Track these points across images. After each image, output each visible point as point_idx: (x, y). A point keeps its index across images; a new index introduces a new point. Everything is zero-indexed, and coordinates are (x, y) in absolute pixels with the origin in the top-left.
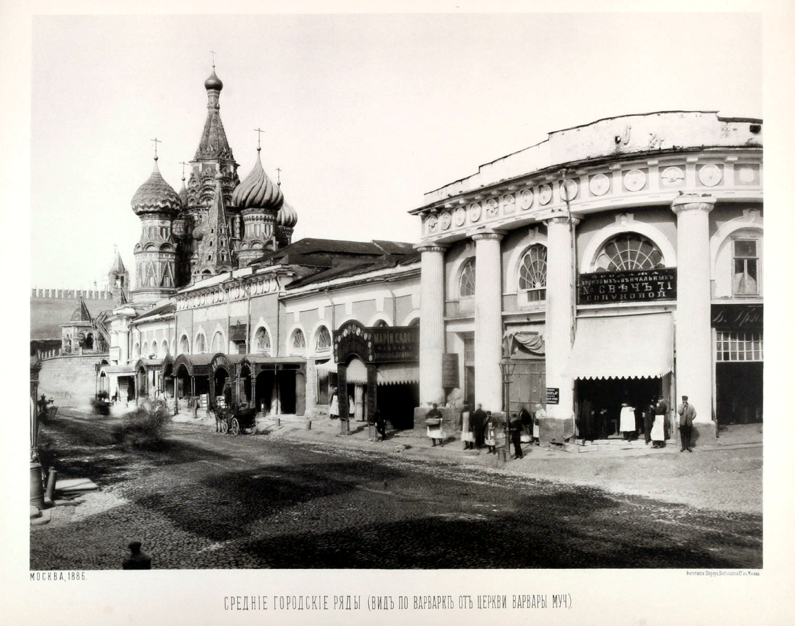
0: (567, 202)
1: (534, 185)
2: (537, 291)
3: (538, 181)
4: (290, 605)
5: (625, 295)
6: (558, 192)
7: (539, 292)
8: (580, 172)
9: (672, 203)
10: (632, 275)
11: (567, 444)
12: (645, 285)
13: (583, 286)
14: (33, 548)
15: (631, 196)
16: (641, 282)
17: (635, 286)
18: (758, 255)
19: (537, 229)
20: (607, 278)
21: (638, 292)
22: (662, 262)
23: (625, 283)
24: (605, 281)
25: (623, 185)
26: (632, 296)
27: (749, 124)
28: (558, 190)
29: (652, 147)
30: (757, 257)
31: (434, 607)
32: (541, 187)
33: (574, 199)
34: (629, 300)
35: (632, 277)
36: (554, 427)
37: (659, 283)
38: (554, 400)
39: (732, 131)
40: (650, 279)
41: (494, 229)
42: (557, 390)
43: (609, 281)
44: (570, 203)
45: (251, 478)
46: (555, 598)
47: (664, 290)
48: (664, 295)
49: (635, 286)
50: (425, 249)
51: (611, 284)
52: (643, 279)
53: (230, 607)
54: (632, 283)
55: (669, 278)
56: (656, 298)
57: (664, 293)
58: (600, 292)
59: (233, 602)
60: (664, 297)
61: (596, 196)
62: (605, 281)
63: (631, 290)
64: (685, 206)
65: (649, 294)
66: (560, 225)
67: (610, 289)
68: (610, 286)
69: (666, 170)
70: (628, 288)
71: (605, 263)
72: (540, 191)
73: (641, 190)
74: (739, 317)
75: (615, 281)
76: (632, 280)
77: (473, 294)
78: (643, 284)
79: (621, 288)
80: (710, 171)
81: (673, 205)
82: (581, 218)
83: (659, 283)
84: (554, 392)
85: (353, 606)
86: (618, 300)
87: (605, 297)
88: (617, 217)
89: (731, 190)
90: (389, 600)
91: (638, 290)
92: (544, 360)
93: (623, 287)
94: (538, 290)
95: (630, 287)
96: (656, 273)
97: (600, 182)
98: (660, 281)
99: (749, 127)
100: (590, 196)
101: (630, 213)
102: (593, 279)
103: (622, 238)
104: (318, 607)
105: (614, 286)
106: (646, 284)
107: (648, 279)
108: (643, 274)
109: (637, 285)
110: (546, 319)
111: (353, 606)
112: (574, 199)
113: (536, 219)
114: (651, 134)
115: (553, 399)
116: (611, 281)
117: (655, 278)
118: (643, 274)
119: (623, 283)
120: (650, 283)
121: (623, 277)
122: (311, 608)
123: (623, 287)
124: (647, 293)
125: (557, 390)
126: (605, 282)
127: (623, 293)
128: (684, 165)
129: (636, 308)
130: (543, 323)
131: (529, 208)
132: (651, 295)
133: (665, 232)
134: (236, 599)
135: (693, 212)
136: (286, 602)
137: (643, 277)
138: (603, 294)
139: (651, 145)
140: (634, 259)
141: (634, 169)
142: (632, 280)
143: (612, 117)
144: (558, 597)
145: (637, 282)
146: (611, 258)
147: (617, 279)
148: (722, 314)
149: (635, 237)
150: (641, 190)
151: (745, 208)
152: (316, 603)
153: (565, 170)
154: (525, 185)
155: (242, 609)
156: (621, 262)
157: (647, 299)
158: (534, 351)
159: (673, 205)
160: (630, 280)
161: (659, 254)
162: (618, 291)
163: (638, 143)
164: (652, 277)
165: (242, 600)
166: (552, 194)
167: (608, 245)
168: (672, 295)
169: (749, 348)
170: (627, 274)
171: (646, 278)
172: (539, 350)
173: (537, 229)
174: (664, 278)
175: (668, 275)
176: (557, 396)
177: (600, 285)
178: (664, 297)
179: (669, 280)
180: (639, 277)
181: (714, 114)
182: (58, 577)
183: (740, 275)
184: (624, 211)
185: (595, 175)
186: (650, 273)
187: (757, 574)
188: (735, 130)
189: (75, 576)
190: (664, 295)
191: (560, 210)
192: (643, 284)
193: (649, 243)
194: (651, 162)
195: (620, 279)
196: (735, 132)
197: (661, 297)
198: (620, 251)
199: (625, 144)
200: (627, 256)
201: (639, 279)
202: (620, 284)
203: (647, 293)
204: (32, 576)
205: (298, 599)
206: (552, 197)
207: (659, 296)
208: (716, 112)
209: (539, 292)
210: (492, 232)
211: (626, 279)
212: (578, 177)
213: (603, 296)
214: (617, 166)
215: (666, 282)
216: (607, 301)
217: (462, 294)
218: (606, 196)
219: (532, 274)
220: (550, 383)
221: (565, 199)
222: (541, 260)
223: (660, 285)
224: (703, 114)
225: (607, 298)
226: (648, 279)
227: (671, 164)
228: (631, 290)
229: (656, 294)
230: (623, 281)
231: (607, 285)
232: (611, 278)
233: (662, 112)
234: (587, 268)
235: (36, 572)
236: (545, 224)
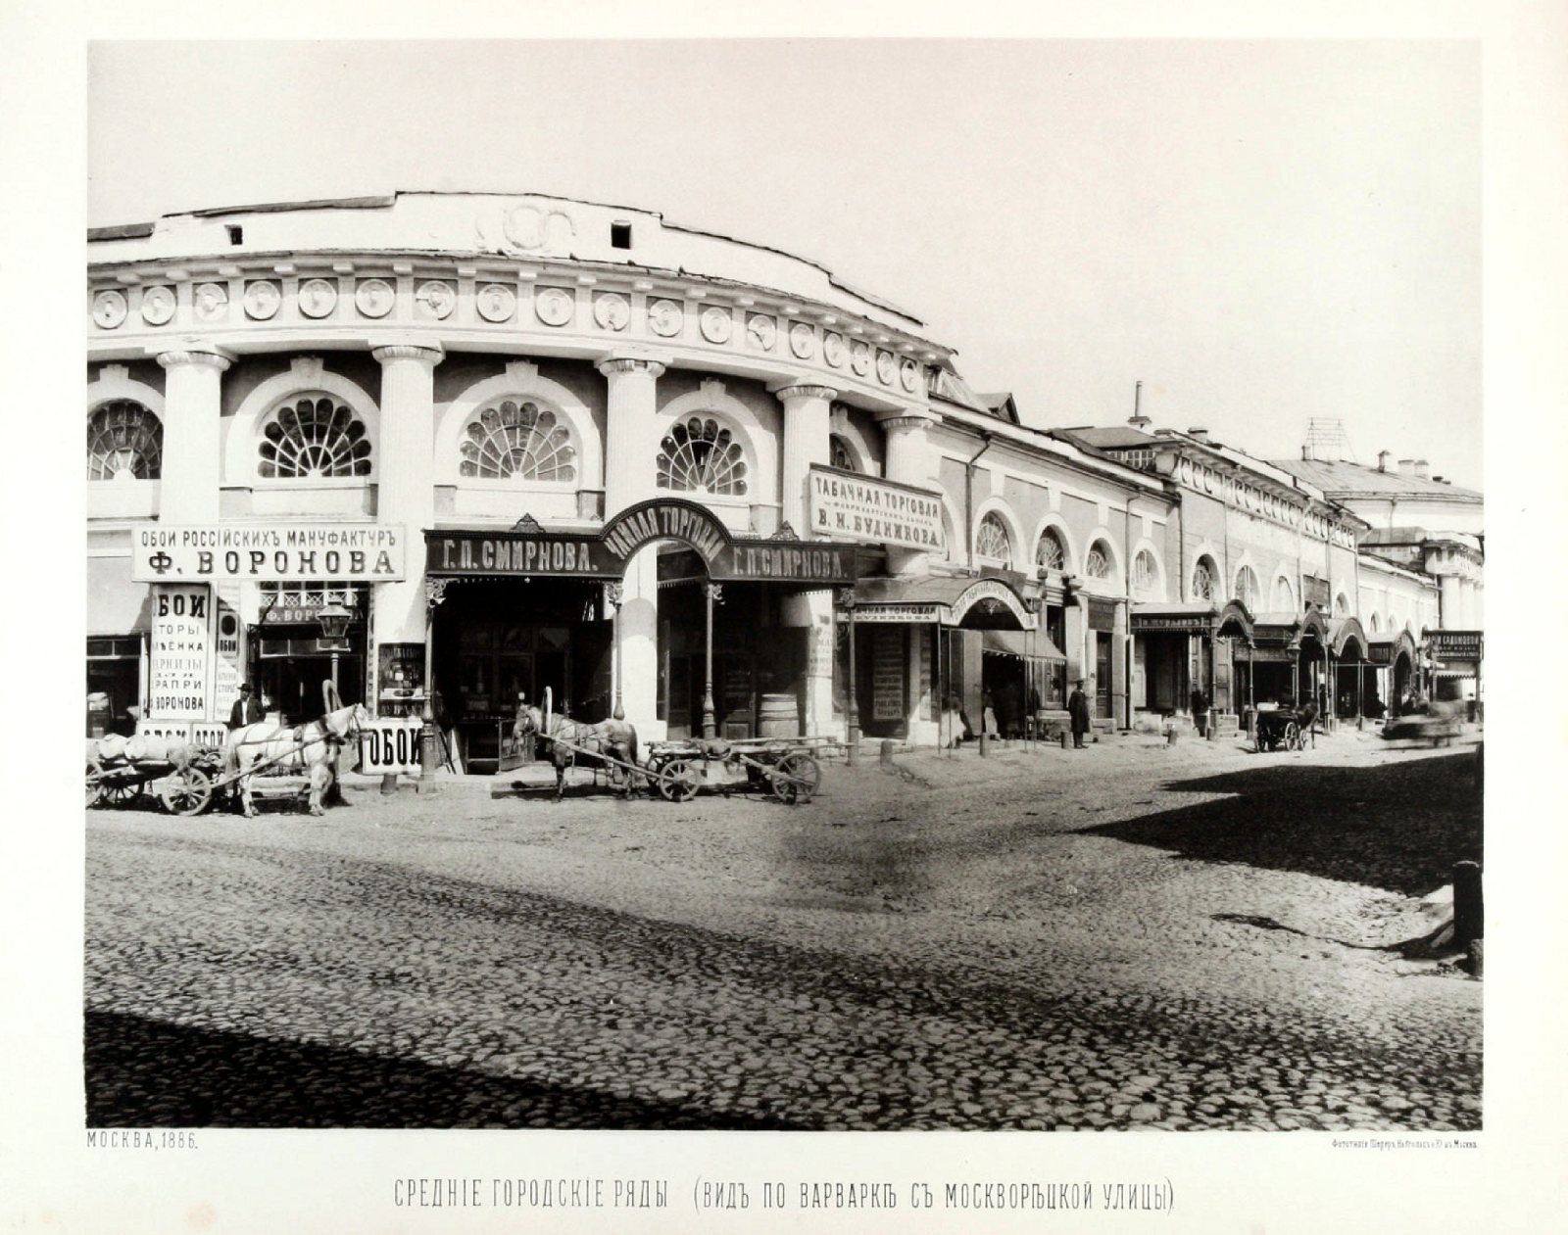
4: (525, 1199)
9: (795, 379)
14: (100, 997)
28: (526, 300)
41: (222, 348)
45: (1181, 850)
46: (951, 1191)
50: (413, 350)
53: (405, 1202)
77: (461, 472)
88: (703, 384)
90: (739, 1189)
104: (583, 1202)
111: (738, 1204)
134: (418, 1184)
136: (511, 1192)
152: (583, 1193)
165: (429, 1187)
166: (338, 300)
169: (880, 688)
182: (143, 1142)
187: (1473, 1145)
189: (177, 1139)
210: (214, 351)
217: (468, 468)
235: (98, 1131)
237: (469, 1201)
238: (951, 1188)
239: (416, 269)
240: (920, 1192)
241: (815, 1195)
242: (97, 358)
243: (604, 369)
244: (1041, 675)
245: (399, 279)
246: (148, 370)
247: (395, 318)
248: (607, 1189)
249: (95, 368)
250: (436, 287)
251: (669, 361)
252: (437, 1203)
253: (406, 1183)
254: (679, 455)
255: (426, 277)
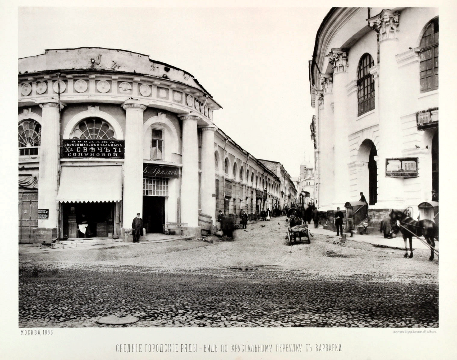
0: (59, 94)
1: (33, 81)
2: (28, 149)
3: (36, 79)
4: (155, 350)
5: (93, 154)
6: (53, 87)
7: (29, 150)
8: (69, 76)
10: (98, 142)
11: (54, 244)
12: (106, 149)
13: (65, 147)
15: (100, 95)
16: (104, 147)
17: (100, 149)
18: (163, 139)
19: (30, 109)
20: (82, 143)
21: (101, 152)
22: (114, 137)
23: (94, 147)
24: (81, 144)
25: (74, 89)
26: (98, 155)
27: (164, 66)
29: (113, 69)
30: (163, 139)
31: (249, 351)
32: (38, 83)
33: (63, 92)
34: (95, 157)
35: (98, 143)
36: (44, 233)
37: (114, 148)
38: (45, 217)
39: (156, 68)
40: (109, 145)
42: (47, 210)
43: (83, 145)
44: (60, 94)
47: (117, 153)
48: (116, 156)
49: (100, 149)
51: (84, 147)
52: (105, 145)
54: (98, 147)
55: (120, 145)
56: (112, 157)
57: (116, 154)
58: (77, 151)
59: (120, 348)
60: (116, 157)
61: (78, 92)
62: (81, 144)
63: (97, 151)
64: (133, 105)
65: (108, 154)
66: (52, 108)
67: (84, 149)
68: (84, 148)
69: (122, 83)
70: (95, 150)
71: (79, 134)
72: (37, 85)
73: (106, 93)
74: (155, 171)
75: (87, 145)
76: (98, 145)
78: (105, 148)
79: (91, 149)
80: (145, 89)
81: (125, 104)
82: (66, 105)
83: (114, 148)
84: (45, 212)
85: (193, 350)
86: (89, 156)
87: (80, 154)
89: (155, 100)
90: (214, 346)
91: (101, 151)
92: (38, 192)
93: (92, 149)
94: (28, 149)
95: (97, 149)
96: (112, 142)
97: (81, 84)
98: (115, 147)
99: (164, 68)
100: (53, 93)
101: (97, 106)
102: (73, 143)
103: (90, 120)
104: (172, 351)
105: (87, 148)
106: (107, 148)
107: (108, 145)
108: (105, 142)
109: (101, 148)
110: (40, 166)
112: (63, 92)
113: (35, 103)
114: (113, 61)
115: (44, 216)
116: (85, 145)
117: (112, 145)
118: (105, 142)
119: (92, 147)
120: (109, 148)
121: (92, 143)
122: (168, 351)
123: (92, 149)
124: (106, 154)
125: (47, 210)
126: (81, 145)
127: (92, 153)
128: (111, 81)
129: (99, 162)
130: (37, 168)
131: (29, 95)
132: (109, 155)
133: (118, 120)
135: (137, 109)
137: (105, 144)
138: (79, 152)
139: (113, 68)
140: (97, 134)
141: (81, 79)
142: (98, 145)
143: (142, 53)
144: (269, 346)
145: (101, 147)
146: (83, 132)
147: (89, 144)
148: (146, 169)
149: (99, 120)
150: (106, 93)
151: (160, 112)
153: (59, 73)
154: (27, 80)
155: (127, 352)
156: (89, 135)
157: (107, 157)
158: (28, 187)
159: (125, 104)
160: (97, 145)
161: (112, 132)
162: (89, 151)
163: (106, 64)
164: (110, 144)
165: (126, 347)
167: (81, 124)
168: (121, 156)
170: (95, 141)
171: (106, 144)
172: (29, 186)
173: (30, 109)
174: (117, 145)
175: (120, 144)
176: (47, 214)
177: (77, 147)
178: (116, 157)
179: (120, 147)
180: (102, 144)
181: (148, 57)
183: (154, 148)
184: (94, 104)
185: (77, 80)
186: (109, 142)
188: (157, 68)
190: (116, 156)
191: (53, 98)
192: (105, 148)
193: (107, 125)
194: (114, 77)
195: (91, 144)
196: (157, 69)
197: (115, 156)
198: (88, 128)
199: (98, 64)
200: (93, 132)
201: (102, 145)
202: (91, 147)
203: (106, 154)
204: (22, 332)
205: (152, 345)
206: (47, 90)
207: (114, 155)
208: (149, 56)
209: (29, 150)
211: (95, 144)
212: (89, 79)
213: (79, 154)
214: (93, 76)
215: (118, 148)
216: (82, 157)
218: (85, 94)
219: (24, 138)
220: (42, 205)
221: (58, 92)
222: (31, 130)
223: (115, 149)
224: (142, 56)
225: (81, 155)
226: (108, 145)
227: (125, 80)
228: (97, 151)
229: (112, 155)
230: (92, 145)
231: (82, 147)
232: (85, 143)
233: (120, 50)
234: (66, 137)
236: (41, 106)
237: (138, 351)
238: (267, 346)
239: (96, 77)
240: (308, 347)
241: (319, 348)
242: (22, 105)
243: (125, 107)
244: (276, 191)
245: (68, 80)
246: (36, 108)
247: (67, 93)
248: (179, 347)
249: (21, 109)
250: (126, 84)
251: (148, 104)
252: (129, 351)
253: (119, 345)
254: (87, 131)
255: (123, 81)
